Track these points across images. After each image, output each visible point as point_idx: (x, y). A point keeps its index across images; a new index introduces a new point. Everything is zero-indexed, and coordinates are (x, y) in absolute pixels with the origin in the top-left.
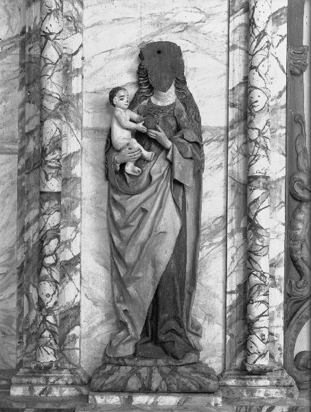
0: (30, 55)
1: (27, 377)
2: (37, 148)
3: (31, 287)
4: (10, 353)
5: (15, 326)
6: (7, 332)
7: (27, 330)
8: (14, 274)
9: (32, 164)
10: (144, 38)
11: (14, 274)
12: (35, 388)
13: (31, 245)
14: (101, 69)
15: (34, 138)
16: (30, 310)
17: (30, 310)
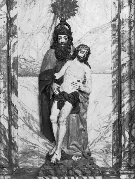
0: (123, 31)
1: (126, 170)
2: (127, 71)
3: (125, 131)
4: (110, 160)
5: (111, 149)
6: (109, 152)
7: (124, 150)
8: (111, 126)
9: (125, 79)
10: (42, 41)
11: (111, 126)
12: (132, 175)
13: (125, 113)
14: (76, 43)
15: (126, 67)
16: (125, 141)
17: (125, 141)
